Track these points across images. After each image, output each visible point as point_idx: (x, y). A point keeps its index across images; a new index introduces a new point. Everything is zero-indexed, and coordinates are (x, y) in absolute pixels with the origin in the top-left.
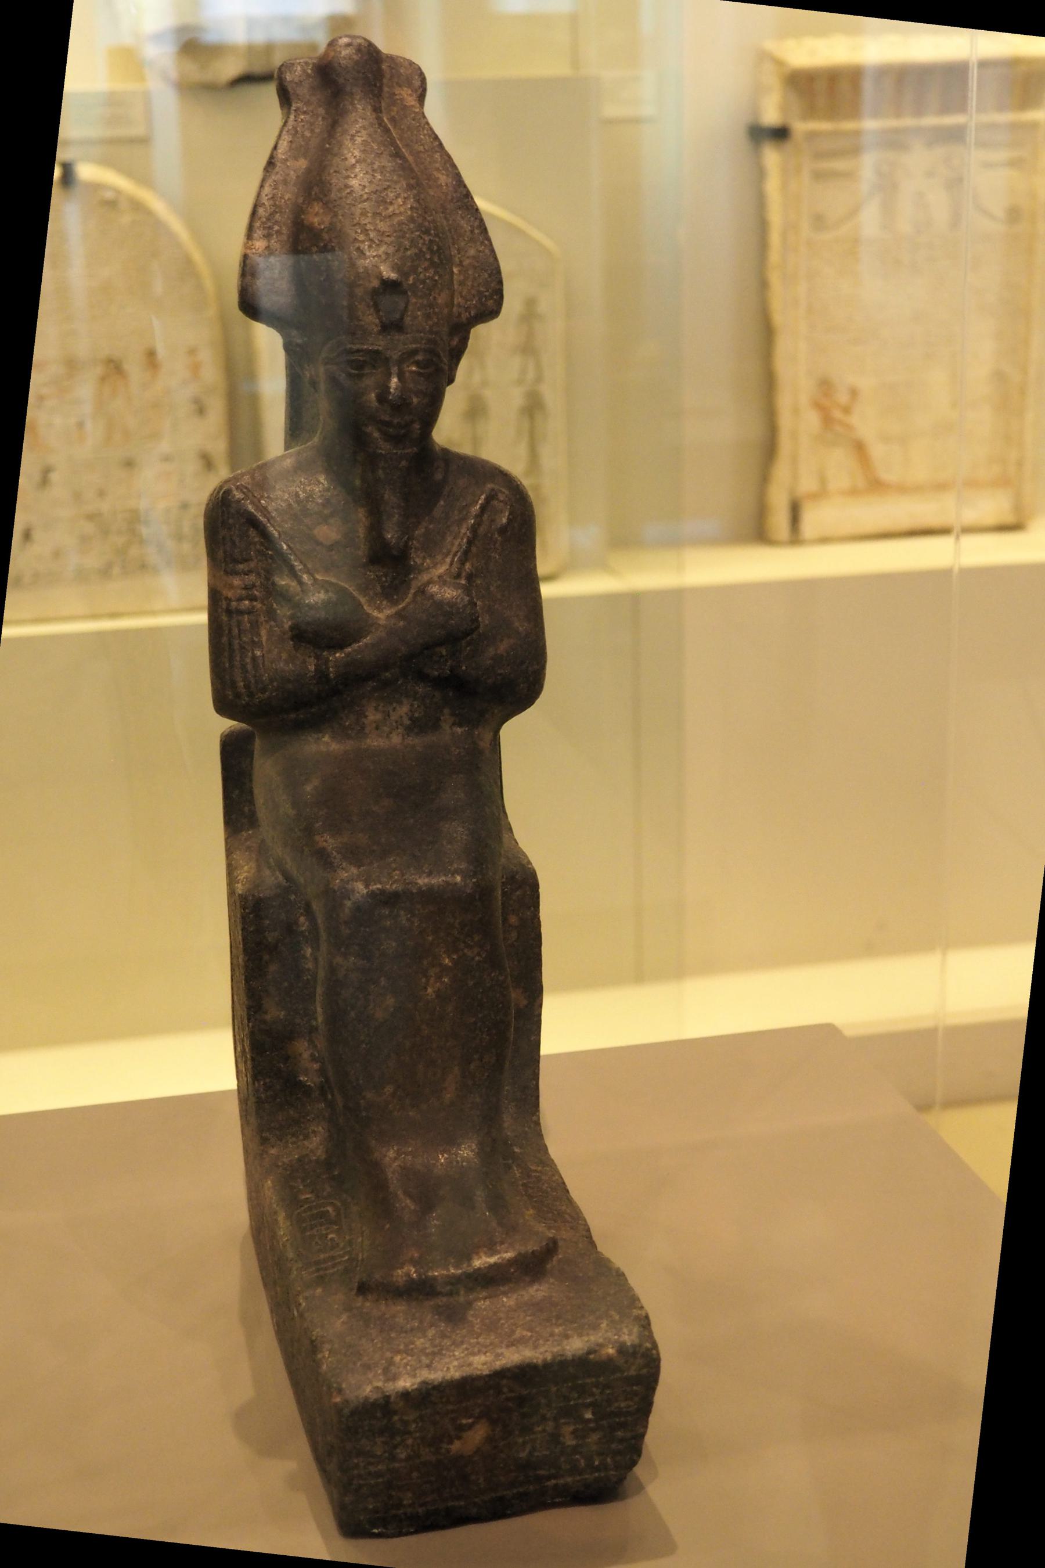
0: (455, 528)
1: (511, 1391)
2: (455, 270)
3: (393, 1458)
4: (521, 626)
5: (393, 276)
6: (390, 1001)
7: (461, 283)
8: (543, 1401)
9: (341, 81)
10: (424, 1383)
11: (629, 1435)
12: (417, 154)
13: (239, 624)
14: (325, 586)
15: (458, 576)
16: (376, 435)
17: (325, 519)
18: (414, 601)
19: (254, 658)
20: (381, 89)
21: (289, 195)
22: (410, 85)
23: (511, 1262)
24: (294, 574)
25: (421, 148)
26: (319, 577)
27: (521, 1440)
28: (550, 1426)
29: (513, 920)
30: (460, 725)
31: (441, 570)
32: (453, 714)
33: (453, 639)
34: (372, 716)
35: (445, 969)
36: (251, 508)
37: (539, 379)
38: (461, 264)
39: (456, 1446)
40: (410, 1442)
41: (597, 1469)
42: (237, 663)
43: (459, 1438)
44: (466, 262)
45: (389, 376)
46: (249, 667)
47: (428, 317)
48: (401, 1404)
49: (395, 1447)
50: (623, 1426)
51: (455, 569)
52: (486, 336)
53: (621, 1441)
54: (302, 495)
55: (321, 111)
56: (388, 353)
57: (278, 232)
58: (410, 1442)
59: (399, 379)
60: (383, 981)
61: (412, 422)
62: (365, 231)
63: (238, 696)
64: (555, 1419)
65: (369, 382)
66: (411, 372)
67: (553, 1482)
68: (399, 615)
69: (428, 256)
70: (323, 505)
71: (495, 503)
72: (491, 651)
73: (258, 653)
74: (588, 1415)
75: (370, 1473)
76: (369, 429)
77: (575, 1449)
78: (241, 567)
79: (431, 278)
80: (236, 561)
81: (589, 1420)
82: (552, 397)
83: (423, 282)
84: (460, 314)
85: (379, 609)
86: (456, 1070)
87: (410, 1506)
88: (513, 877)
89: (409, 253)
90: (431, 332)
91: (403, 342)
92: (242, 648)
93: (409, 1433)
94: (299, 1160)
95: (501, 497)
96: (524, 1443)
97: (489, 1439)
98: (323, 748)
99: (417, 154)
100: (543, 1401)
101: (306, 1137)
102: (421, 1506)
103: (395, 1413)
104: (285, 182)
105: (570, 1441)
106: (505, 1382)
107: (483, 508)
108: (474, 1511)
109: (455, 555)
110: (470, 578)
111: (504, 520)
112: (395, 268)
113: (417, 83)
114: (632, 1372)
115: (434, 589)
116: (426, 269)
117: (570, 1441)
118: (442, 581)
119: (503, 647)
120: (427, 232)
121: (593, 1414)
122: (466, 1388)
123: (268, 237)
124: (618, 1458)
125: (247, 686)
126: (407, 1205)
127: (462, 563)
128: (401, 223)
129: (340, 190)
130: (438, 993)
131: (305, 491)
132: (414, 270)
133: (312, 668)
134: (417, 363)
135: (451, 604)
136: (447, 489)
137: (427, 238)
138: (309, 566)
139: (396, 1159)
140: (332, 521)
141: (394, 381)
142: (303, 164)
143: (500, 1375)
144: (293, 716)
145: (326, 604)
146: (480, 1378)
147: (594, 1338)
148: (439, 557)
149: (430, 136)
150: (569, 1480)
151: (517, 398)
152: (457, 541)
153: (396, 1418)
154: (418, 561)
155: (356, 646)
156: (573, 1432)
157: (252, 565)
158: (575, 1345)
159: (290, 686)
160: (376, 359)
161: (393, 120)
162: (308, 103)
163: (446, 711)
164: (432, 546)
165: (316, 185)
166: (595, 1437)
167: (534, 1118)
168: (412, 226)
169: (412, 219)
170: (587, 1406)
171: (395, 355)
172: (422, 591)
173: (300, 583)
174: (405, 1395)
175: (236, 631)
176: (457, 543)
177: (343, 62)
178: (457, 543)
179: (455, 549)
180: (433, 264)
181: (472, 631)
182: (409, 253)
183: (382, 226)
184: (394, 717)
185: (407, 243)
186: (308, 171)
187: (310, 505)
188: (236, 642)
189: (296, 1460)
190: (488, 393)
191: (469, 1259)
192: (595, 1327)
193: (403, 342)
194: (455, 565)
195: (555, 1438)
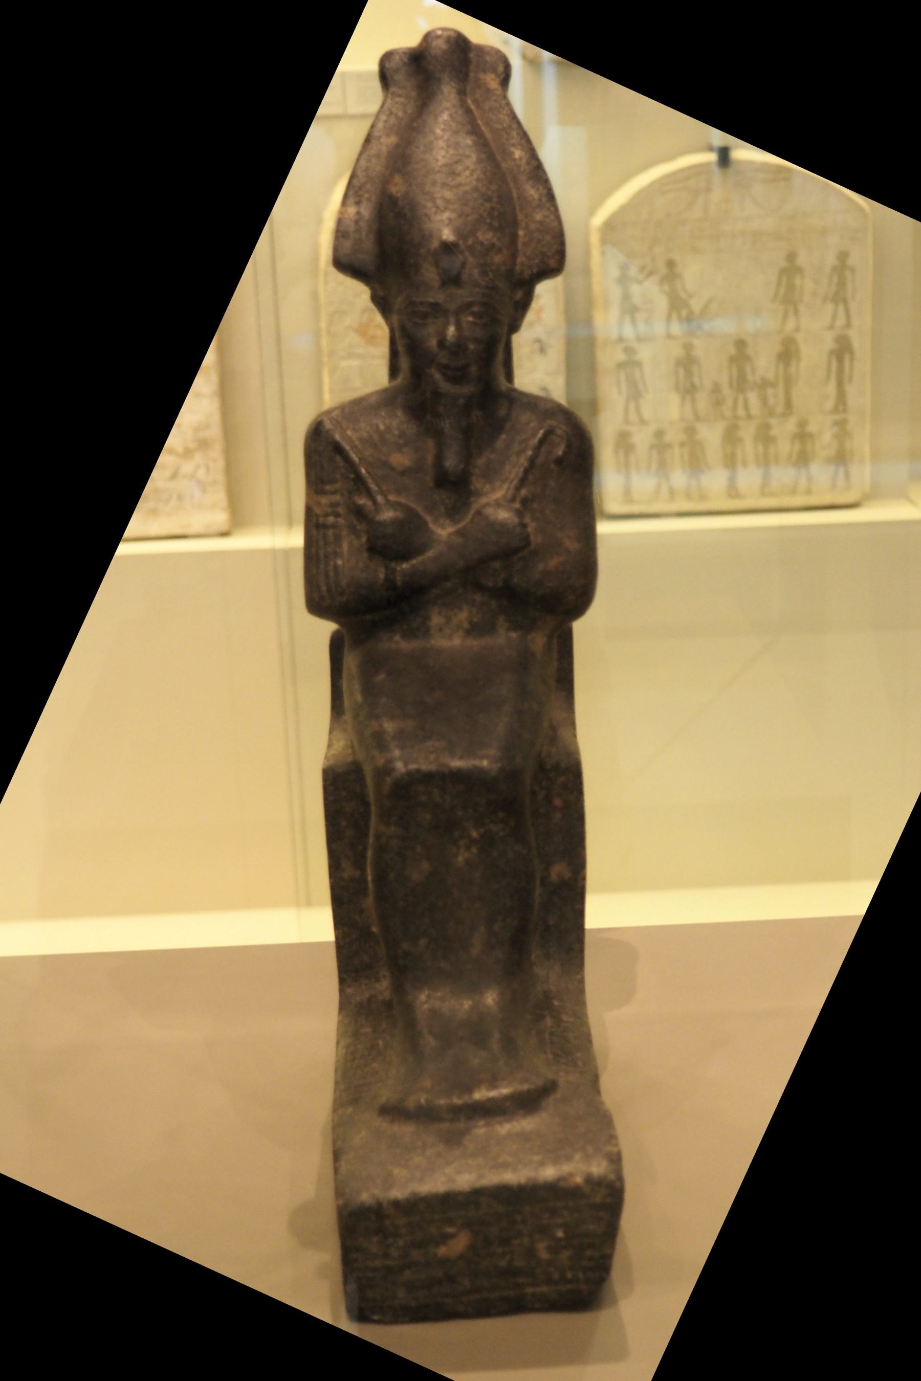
0: (514, 459)
2: (521, 233)
3: (386, 1256)
4: (572, 545)
6: (425, 866)
7: (525, 244)
9: (431, 68)
10: (414, 1194)
13: (325, 536)
14: (394, 506)
15: (513, 500)
17: (399, 448)
18: (472, 521)
19: (336, 567)
21: (378, 167)
22: (494, 71)
23: (506, 1098)
24: (370, 495)
25: (499, 126)
27: (500, 1250)
28: (526, 1241)
29: (558, 802)
31: (499, 494)
34: (436, 620)
35: (473, 842)
36: (337, 437)
37: (848, 325)
38: (527, 227)
39: (442, 1251)
46: (332, 574)
51: (509, 496)
52: (546, 292)
53: (591, 1259)
54: (382, 427)
55: (414, 94)
59: (456, 329)
60: (419, 849)
65: (431, 329)
66: (469, 322)
68: (459, 533)
69: (488, 220)
71: (553, 437)
72: (541, 567)
73: (339, 562)
74: (560, 1234)
78: (328, 488)
80: (323, 482)
82: (860, 342)
89: (470, 218)
91: (463, 295)
92: (326, 557)
94: (369, 1000)
95: (559, 432)
98: (394, 646)
101: (377, 980)
107: (542, 441)
108: (461, 1308)
109: (511, 482)
110: (525, 502)
112: (458, 232)
113: (501, 69)
114: (598, 1199)
115: (489, 511)
117: (544, 1255)
118: (498, 504)
119: (553, 563)
120: (489, 199)
121: (565, 1232)
122: (447, 1203)
123: (358, 203)
125: (329, 590)
126: (429, 1042)
127: (518, 489)
128: (466, 192)
130: (467, 862)
131: (384, 424)
133: (382, 576)
134: (474, 314)
135: (503, 525)
138: (384, 488)
139: (426, 1002)
140: (405, 450)
141: (451, 330)
142: (393, 140)
143: (477, 1195)
145: (394, 521)
146: (460, 1193)
147: (566, 1168)
148: (498, 484)
149: (508, 116)
151: (829, 343)
152: (514, 469)
155: (420, 558)
157: (338, 486)
158: (549, 1173)
160: (437, 310)
161: (476, 102)
164: (490, 474)
165: (401, 160)
166: (566, 1254)
167: (578, 977)
168: (475, 195)
169: (476, 189)
171: (453, 306)
172: (479, 513)
173: (375, 502)
174: (396, 1203)
175: (321, 543)
176: (514, 471)
177: (433, 52)
178: (514, 471)
179: (512, 476)
181: (524, 547)
182: (470, 218)
183: (448, 194)
187: (388, 436)
188: (322, 553)
189: (328, 1255)
190: (800, 337)
191: (470, 1090)
192: (569, 1158)
193: (463, 295)
195: (531, 1252)
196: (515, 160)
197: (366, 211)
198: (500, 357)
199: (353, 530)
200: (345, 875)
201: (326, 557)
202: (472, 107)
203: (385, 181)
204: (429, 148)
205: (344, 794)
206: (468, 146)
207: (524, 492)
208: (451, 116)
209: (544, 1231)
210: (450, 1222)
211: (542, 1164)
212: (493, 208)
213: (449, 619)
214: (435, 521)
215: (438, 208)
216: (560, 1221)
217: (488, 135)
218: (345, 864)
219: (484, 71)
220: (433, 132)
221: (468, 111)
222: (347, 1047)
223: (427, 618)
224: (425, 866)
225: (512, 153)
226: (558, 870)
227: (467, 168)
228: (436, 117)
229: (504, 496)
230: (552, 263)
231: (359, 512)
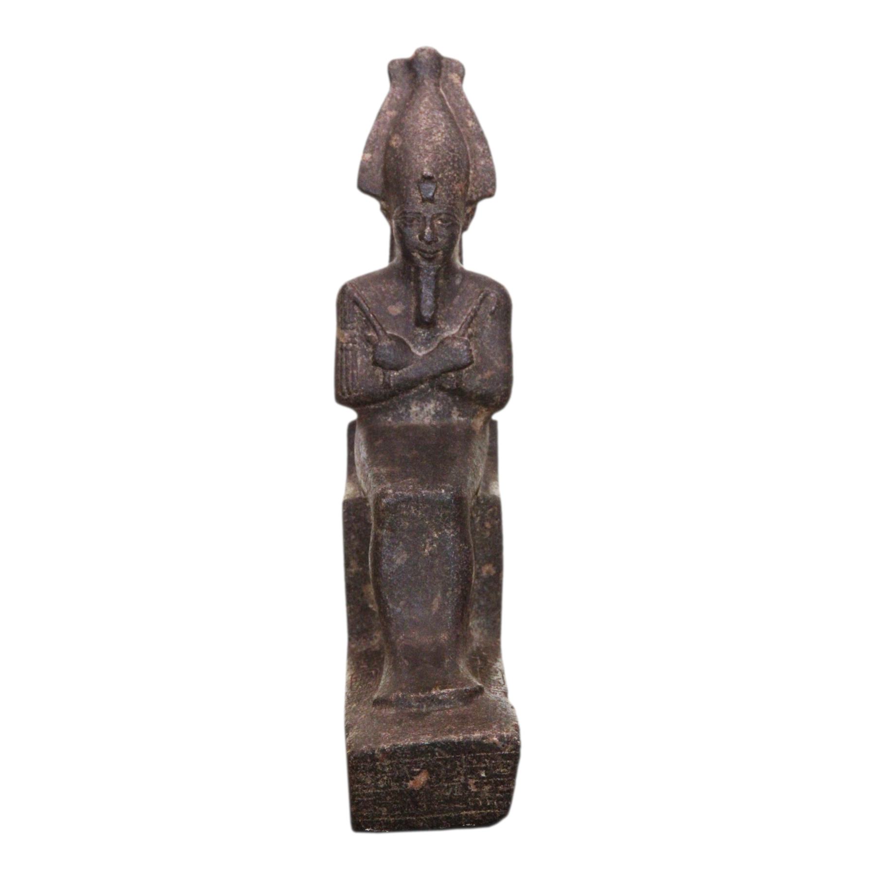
0: (464, 310)
1: (440, 755)
2: (471, 172)
4: (498, 364)
5: (429, 174)
8: (458, 763)
11: (506, 789)
12: (456, 109)
16: (419, 257)
20: (440, 74)
26: (388, 332)
29: (488, 525)
30: (463, 416)
32: (458, 410)
33: (457, 368)
35: (435, 540)
36: (355, 295)
38: (475, 169)
39: (411, 784)
40: (385, 778)
41: (489, 808)
42: (344, 377)
43: (412, 779)
44: (478, 168)
45: (425, 226)
46: (350, 378)
47: (448, 196)
48: (381, 755)
49: (378, 780)
50: (502, 783)
51: (461, 332)
53: (501, 792)
55: (407, 85)
56: (425, 215)
57: (378, 149)
58: (385, 778)
61: (437, 251)
62: (419, 150)
63: (343, 394)
64: (465, 775)
67: (465, 813)
70: (394, 295)
74: (483, 775)
75: (364, 794)
76: (415, 254)
77: (476, 794)
79: (452, 175)
81: (483, 778)
83: (447, 177)
84: (471, 196)
85: (420, 351)
86: (439, 595)
87: (386, 816)
88: (488, 501)
90: (450, 204)
93: (385, 772)
96: (448, 787)
97: (429, 782)
99: (456, 109)
100: (458, 763)
102: (392, 817)
103: (378, 760)
104: (384, 123)
105: (473, 789)
106: (436, 749)
111: (493, 308)
112: (434, 170)
116: (450, 171)
117: (473, 789)
120: (453, 151)
124: (501, 802)
125: (348, 389)
129: (409, 127)
130: (430, 552)
132: (443, 171)
134: (441, 220)
136: (462, 289)
137: (451, 154)
138: (384, 326)
141: (428, 230)
144: (372, 407)
150: (473, 812)
153: (378, 763)
154: (442, 326)
156: (476, 784)
157: (355, 324)
159: (370, 390)
161: (446, 91)
162: (401, 81)
163: (455, 408)
164: (450, 318)
166: (487, 788)
170: (482, 769)
175: (344, 360)
180: (453, 168)
183: (427, 147)
184: (426, 409)
185: (440, 156)
186: (397, 117)
188: (344, 365)
191: (430, 690)
194: (463, 330)
195: (465, 786)
196: (468, 127)
197: (378, 157)
198: (457, 248)
199: (364, 352)
200: (353, 570)
201: (347, 368)
202: (443, 94)
203: (389, 138)
204: (416, 119)
205: (353, 518)
206: (441, 118)
207: (470, 330)
208: (430, 99)
209: (473, 771)
210: (416, 765)
211: (474, 730)
212: (454, 156)
213: (422, 409)
214: (415, 346)
215: (421, 155)
216: (483, 765)
217: (452, 111)
218: (353, 563)
219: (452, 71)
220: (418, 108)
221: (441, 96)
222: (352, 675)
223: (408, 407)
224: (405, 556)
225: (467, 123)
226: (487, 569)
227: (439, 131)
228: (420, 101)
229: (458, 333)
230: (490, 190)
231: (368, 340)
